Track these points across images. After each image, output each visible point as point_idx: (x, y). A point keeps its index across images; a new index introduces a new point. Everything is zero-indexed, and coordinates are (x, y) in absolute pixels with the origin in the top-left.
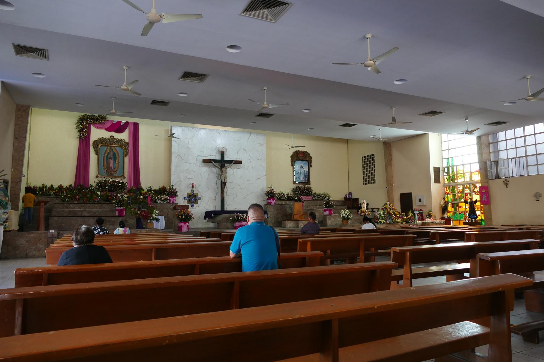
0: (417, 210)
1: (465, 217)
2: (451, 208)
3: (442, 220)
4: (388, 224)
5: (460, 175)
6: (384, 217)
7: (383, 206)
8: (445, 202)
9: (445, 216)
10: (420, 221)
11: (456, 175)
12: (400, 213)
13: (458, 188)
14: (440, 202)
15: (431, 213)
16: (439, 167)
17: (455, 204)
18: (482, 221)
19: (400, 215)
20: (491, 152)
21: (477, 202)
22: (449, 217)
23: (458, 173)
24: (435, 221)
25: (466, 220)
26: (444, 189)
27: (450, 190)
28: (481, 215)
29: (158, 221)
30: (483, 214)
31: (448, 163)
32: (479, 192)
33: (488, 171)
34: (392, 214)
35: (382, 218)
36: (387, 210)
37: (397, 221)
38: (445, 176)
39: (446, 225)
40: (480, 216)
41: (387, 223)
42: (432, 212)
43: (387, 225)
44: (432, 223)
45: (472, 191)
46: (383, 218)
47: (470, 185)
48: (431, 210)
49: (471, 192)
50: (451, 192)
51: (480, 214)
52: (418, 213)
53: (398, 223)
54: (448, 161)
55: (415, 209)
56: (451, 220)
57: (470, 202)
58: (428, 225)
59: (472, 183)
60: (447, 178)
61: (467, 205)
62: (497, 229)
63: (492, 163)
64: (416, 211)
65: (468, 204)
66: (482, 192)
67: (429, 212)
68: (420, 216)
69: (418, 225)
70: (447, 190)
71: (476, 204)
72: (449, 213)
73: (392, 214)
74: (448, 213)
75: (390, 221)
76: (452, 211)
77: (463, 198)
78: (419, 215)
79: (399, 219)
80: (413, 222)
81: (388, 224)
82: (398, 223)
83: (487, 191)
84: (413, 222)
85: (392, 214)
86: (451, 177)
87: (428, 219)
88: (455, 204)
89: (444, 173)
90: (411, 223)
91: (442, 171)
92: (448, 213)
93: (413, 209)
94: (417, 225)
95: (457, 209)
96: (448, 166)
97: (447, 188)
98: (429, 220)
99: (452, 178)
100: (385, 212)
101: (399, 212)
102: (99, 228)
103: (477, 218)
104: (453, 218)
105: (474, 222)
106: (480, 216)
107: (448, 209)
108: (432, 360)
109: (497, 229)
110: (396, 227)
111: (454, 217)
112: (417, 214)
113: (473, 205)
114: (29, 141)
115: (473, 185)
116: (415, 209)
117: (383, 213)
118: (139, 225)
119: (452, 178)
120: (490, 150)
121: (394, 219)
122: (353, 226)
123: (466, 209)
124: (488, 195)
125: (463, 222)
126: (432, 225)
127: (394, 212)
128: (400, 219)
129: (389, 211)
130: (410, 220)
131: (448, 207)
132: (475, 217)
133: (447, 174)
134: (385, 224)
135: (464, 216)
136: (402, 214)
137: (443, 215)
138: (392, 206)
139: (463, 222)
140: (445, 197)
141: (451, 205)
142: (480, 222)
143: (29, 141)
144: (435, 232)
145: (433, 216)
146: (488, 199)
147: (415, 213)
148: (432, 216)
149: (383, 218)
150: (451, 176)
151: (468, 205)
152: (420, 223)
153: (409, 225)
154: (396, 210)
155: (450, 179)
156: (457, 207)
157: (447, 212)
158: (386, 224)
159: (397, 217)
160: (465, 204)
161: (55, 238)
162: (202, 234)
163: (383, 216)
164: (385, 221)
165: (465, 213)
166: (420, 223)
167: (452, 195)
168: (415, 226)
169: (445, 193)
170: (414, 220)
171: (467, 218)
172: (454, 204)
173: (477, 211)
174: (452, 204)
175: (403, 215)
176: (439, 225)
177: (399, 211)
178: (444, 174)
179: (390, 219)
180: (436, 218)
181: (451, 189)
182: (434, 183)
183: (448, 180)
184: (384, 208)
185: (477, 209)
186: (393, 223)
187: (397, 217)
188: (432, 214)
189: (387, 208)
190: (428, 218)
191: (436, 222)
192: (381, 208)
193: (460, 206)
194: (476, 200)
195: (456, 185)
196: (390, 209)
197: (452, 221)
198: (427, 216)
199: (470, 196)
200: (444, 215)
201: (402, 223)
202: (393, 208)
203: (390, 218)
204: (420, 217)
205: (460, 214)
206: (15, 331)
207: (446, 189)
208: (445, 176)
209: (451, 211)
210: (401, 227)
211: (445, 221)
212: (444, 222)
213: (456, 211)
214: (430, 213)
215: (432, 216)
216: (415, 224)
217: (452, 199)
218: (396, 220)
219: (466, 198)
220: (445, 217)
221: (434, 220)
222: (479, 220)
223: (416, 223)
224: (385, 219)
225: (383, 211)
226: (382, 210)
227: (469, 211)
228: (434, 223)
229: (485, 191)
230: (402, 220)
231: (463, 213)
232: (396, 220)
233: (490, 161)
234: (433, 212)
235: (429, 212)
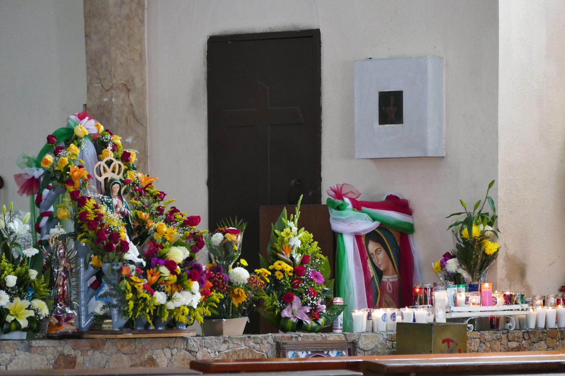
0: (358, 205)
4: (77, 335)
6: (42, 271)
7: (35, 154)
10: (378, 313)
12: (202, 228)
15: (483, 236)
19: (194, 250)
34: (124, 235)
35: (23, 281)
36: (74, 195)
37: (161, 307)
41: (67, 328)
43: (67, 348)
44: (488, 335)
46: (33, 274)
48: (487, 209)
52: (372, 236)
53: (173, 324)
55: (339, 195)
58: (451, 351)
64: (349, 211)
67: (468, 222)
68: (381, 258)
69: (362, 344)
73: (115, 236)
75: (98, 307)
78: (372, 247)
79: (181, 285)
80: (314, 314)
81: (77, 335)
82: (173, 324)
84: (314, 314)
85: (124, 235)
87: (452, 290)
90: (300, 326)
93: (325, 197)
94: (353, 348)
98: (462, 297)
100: (53, 220)
101: (193, 221)
110: (152, 361)
112: (358, 237)
114: (71, 254)
116: (339, 195)
117: (37, 229)
121: (141, 283)
122: (249, 337)
127: (143, 222)
128: (195, 285)
129: (89, 206)
130: (287, 299)
134: (50, 337)
136: (218, 237)
138: (125, 157)
143: (71, 254)
145: (500, 261)
147: (336, 226)
148: (488, 259)
149: (33, 274)
152: (382, 327)
153: (280, 350)
154: (161, 196)
158: (64, 337)
159: (164, 270)
162: (527, 321)
163: (35, 261)
164: (44, 309)
166: (382, 327)
168: (333, 356)
170: (329, 303)
175: (226, 245)
176: (550, 348)
177: (186, 213)
179: (96, 286)
180: (530, 279)
184: (47, 173)
186: (130, 325)
187: (171, 265)
188: (490, 247)
189: (71, 182)
190: (456, 279)
191: (522, 323)
192: (18, 177)
196: (108, 191)
198: (452, 265)
201: (219, 333)
202: (132, 175)
203: (99, 274)
204: (380, 274)
206: (339, 340)
210: (196, 365)
214: (476, 231)
216: (331, 337)
217: (338, 354)
218: (160, 297)
223: (348, 327)
224: (52, 285)
225: (39, 201)
226: (27, 200)
228: (513, 325)
230: (216, 296)
232: (160, 297)
234: (501, 223)
235: (468, 222)
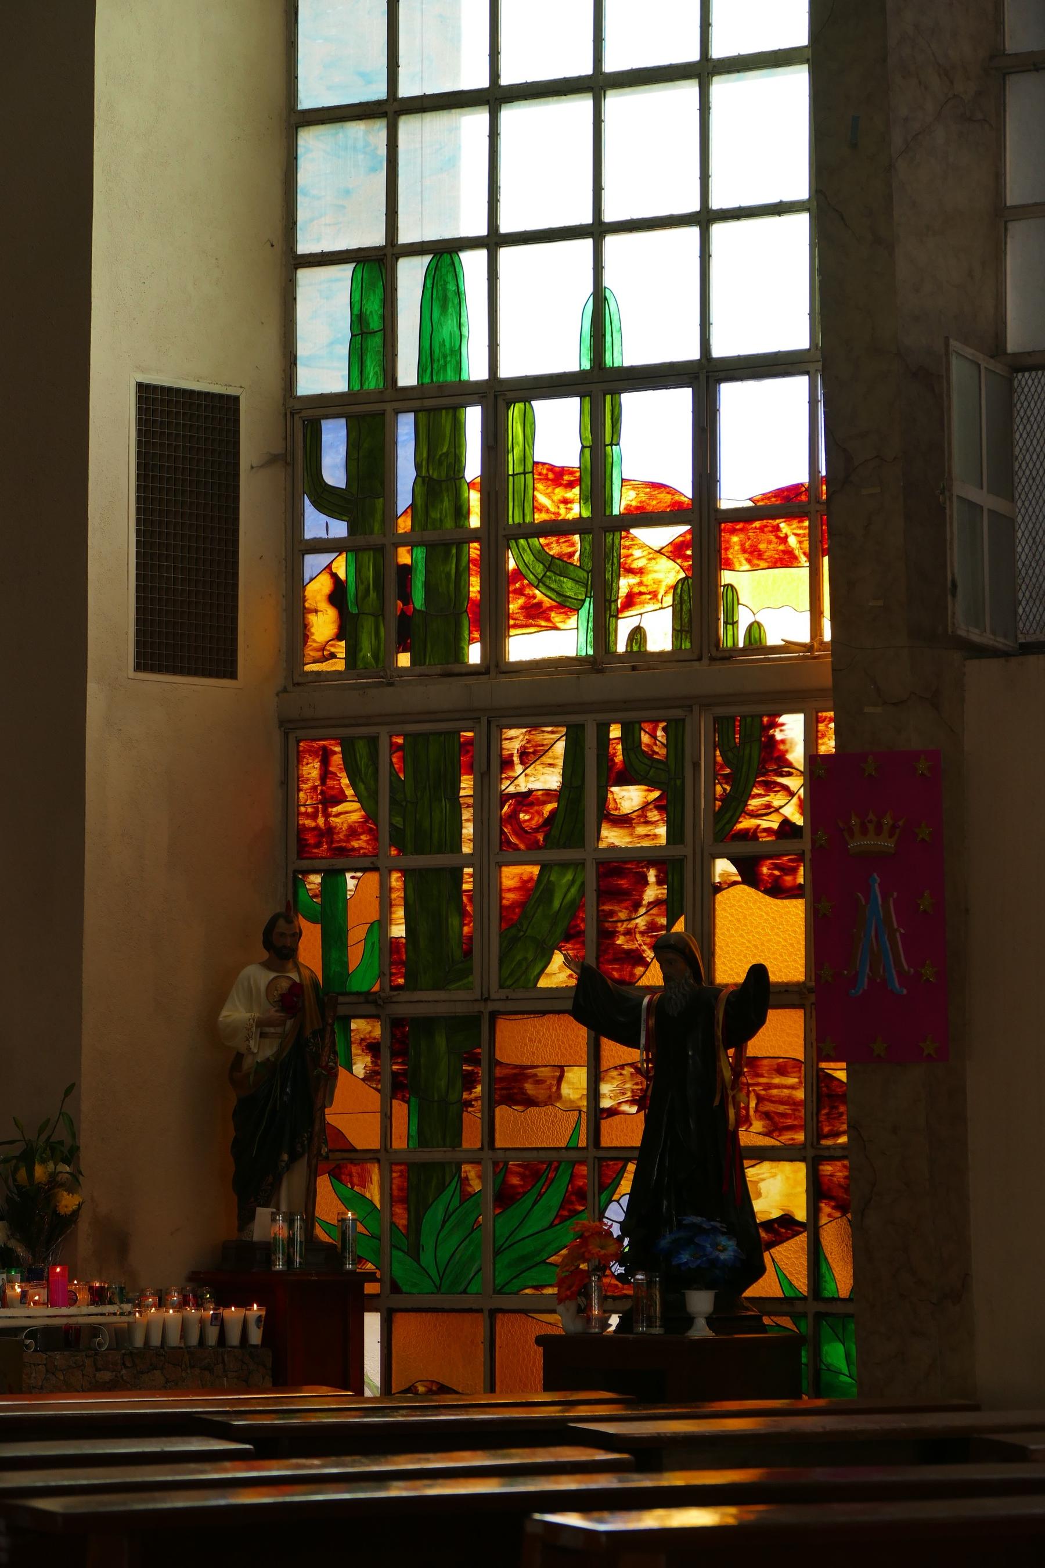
1: (579, 1252)
2: (373, 1098)
3: (223, 1301)
5: (540, 555)
8: (296, 988)
9: (280, 1228)
11: (474, 549)
13: (507, 763)
14: (218, 999)
15: (54, 1182)
16: (236, 399)
17: (441, 1042)
18: (826, 1330)
20: (1013, 197)
21: (774, 1016)
22: (334, 1254)
23: (514, 517)
24: (110, 1314)
25: (584, 1310)
26: (289, 781)
27: (368, 799)
28: (813, 1227)
29: (585, 1162)
30: (842, 1208)
31: (375, 342)
32: (805, 844)
33: (955, 512)
38: (314, 563)
39: (282, 1379)
40: (801, 1240)
42: (71, 1156)
45: (704, 823)
47: (675, 730)
49: (685, 850)
50: (397, 839)
51: (801, 1215)
54: (374, 307)
56: (371, 1304)
57: (658, 1009)
59: (706, 703)
60: (337, 596)
61: (614, 1051)
62: (1019, 1454)
63: (1023, 379)
65: (633, 1043)
66: (856, 844)
67: (28, 1158)
70: (331, 798)
71: (758, 1046)
72: (337, 1174)
74: (324, 1183)
76: (382, 1155)
77: (572, 936)
83: (924, 832)
86: (406, 571)
88: (441, 1042)
89: (309, 509)
91: (272, 460)
92: (324, 1183)
95: (472, 1121)
96: (373, 383)
97: (337, 760)
99: (419, 598)
102: (56, 1165)
103: (759, 1271)
104: (401, 1267)
105: (700, 1330)
106: (801, 1240)
107: (333, 1117)
108: (772, 1317)
109: (1019, 1454)
111: (414, 1251)
113: (711, 1060)
115: (722, 724)
118: (454, 1147)
119: (419, 598)
120: (999, 176)
123: (598, 1115)
124: (926, 903)
125: (540, 1341)
126: (69, 1389)
131: (332, 1076)
132: (727, 1249)
133: (339, 529)
135: (567, 1234)
137: (246, 1218)
139: (540, 1341)
140: (291, 908)
141: (373, 1048)
142: (792, 1344)
144: (71, 1519)
145: (84, 1226)
146: (928, 972)
148: (66, 1222)
150: (404, 557)
151: (634, 1055)
155: (380, 614)
156: (470, 1080)
157: (313, 1175)
160: (581, 1033)
161: (62, 1185)
165: (581, 1195)
167: (396, 880)
169: (303, 849)
171: (602, 1268)
172: (426, 1025)
173: (762, 1155)
174: (395, 1025)
176: (170, 1386)
178: (297, 521)
181: (396, 787)
182: (139, 667)
183: (345, 630)
185: (758, 1125)
188: (68, 1202)
191: (122, 1336)
193: (521, 1073)
194: (758, 972)
195: (471, 716)
197: (372, 1323)
199: (671, 906)
200: (263, 1213)
205: (505, 1198)
207: (312, 770)
208: (314, 563)
209: (372, 1156)
211: (268, 1324)
212: (256, 1336)
213: (437, 1155)
215: (66, 1222)
219: (607, 935)
220: (268, 1248)
221: (98, 1297)
222: (786, 1304)
227: (644, 1154)
228: (104, 1341)
229: (887, 844)
231: (554, 1197)
233: (996, 346)
234: (87, 1157)
